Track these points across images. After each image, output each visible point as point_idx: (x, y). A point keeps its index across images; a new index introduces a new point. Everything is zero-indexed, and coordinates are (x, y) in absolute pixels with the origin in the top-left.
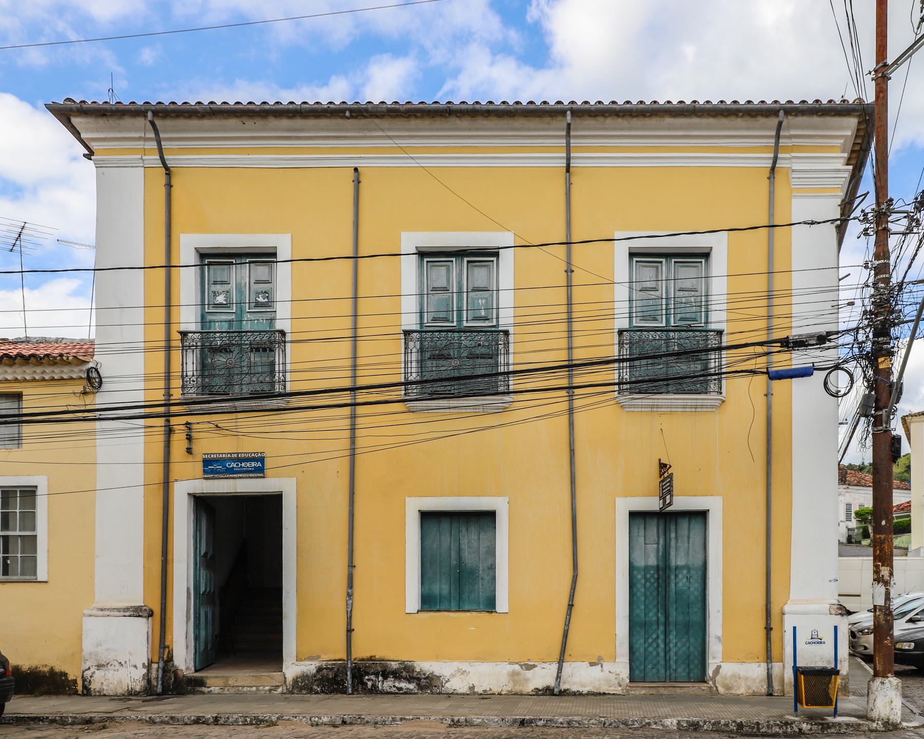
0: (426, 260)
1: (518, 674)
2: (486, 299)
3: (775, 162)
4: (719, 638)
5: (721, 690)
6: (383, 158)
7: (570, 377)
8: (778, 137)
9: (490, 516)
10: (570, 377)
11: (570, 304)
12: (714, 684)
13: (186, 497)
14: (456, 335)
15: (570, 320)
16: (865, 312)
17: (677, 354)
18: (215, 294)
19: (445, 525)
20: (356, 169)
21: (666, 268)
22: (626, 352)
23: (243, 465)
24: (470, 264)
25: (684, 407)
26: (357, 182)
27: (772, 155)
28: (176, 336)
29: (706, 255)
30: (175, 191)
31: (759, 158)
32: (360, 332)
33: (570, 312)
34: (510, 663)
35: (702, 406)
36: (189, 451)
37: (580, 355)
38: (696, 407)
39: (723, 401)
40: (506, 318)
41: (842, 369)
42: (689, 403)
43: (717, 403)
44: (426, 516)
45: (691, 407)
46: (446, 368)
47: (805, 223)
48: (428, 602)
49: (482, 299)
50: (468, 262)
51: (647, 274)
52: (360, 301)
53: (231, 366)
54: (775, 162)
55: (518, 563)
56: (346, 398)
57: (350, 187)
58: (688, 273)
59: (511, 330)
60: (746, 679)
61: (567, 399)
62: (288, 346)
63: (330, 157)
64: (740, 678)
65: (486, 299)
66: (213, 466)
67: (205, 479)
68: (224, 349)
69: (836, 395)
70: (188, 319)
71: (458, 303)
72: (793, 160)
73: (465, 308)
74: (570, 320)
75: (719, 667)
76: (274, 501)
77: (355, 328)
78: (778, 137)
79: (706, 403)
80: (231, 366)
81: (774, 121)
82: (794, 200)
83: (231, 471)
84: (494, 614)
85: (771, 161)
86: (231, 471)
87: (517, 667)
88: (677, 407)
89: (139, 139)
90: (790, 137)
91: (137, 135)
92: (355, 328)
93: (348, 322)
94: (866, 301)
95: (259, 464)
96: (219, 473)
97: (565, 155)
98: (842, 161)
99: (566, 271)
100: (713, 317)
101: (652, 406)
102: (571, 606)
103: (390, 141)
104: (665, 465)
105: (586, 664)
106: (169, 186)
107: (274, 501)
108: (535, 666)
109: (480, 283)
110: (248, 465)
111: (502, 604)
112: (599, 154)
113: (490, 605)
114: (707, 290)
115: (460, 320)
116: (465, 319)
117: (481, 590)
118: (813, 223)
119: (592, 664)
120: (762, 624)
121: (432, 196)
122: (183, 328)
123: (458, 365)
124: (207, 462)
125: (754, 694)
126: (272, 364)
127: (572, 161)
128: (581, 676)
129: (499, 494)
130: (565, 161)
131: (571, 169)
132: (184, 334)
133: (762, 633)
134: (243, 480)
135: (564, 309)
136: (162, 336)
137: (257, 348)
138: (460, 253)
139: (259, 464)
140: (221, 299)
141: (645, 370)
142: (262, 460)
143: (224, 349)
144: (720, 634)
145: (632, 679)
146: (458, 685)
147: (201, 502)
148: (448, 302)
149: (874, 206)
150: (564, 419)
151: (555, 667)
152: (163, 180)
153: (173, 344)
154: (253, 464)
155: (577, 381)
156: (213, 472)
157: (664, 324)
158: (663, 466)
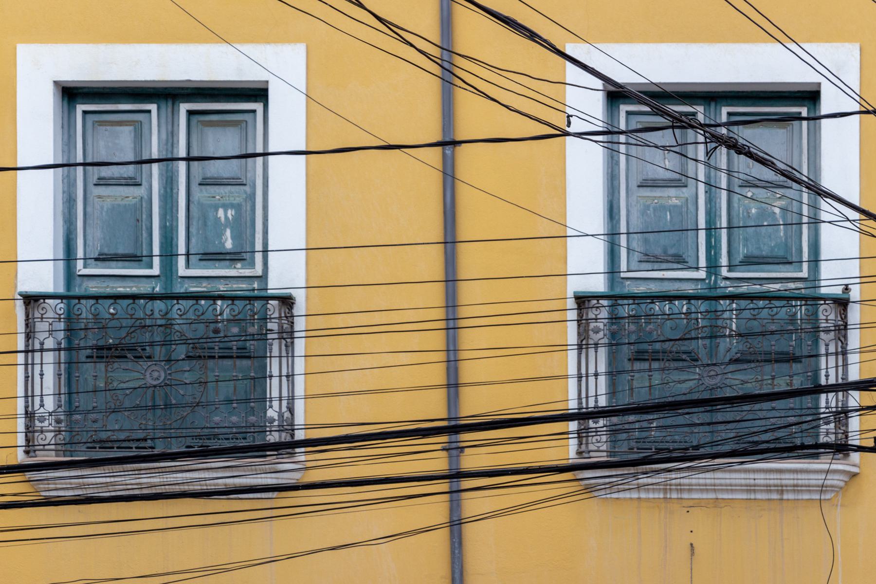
0: (80, 108)
2: (238, 207)
7: (455, 450)
10: (455, 450)
11: (451, 280)
14: (159, 305)
22: (599, 394)
24: (195, 119)
33: (451, 304)
35: (796, 488)
37: (476, 404)
38: (781, 489)
39: (854, 475)
40: (286, 272)
45: (768, 488)
49: (226, 207)
50: (190, 113)
59: (300, 297)
61: (442, 325)
65: (238, 207)
73: (182, 249)
79: (803, 479)
100: (826, 271)
115: (169, 255)
138: (167, 94)
148: (139, 214)
150: (440, 539)
155: (472, 460)
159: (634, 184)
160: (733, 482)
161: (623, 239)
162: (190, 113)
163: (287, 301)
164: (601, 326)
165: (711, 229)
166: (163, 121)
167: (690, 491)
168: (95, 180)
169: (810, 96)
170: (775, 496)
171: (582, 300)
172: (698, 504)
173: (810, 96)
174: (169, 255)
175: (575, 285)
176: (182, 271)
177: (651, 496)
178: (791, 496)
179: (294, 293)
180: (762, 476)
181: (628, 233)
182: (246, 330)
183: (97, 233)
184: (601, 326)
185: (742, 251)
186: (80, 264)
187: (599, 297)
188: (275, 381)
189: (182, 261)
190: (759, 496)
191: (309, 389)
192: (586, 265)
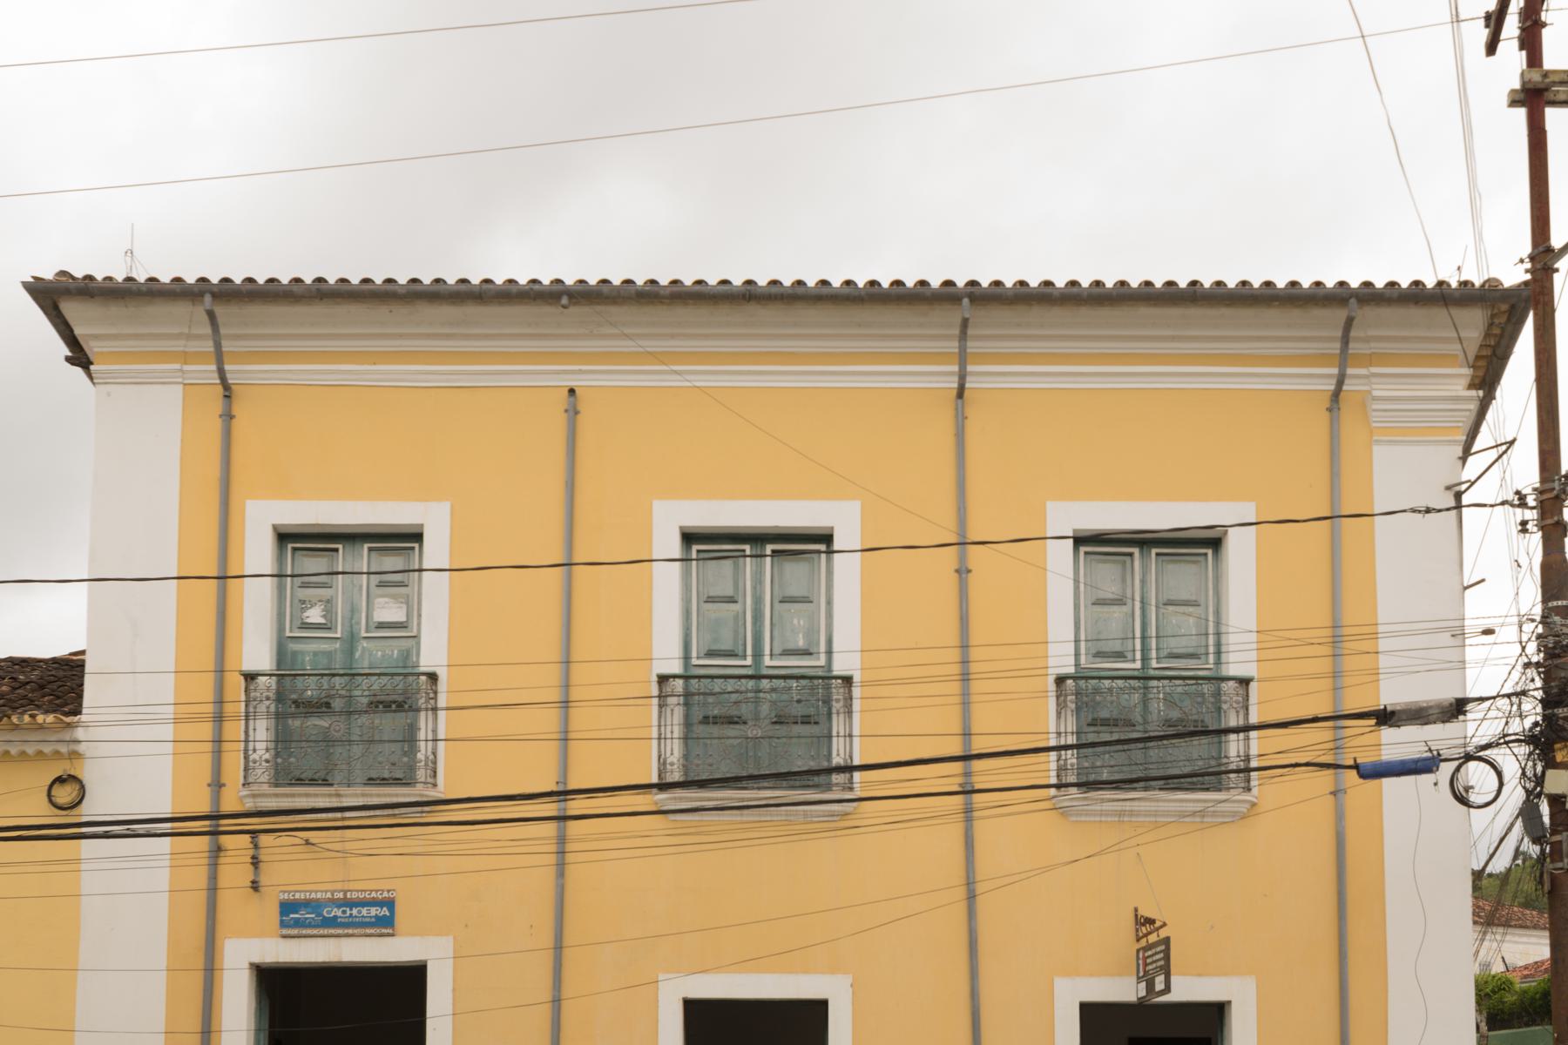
3: (1340, 382)
6: (622, 379)
7: (967, 774)
8: (1345, 340)
15: (965, 677)
16: (1527, 665)
18: (304, 604)
20: (572, 391)
23: (355, 912)
25: (1183, 815)
26: (573, 412)
27: (1335, 371)
28: (236, 685)
30: (240, 426)
32: (575, 694)
36: (255, 886)
39: (1254, 805)
40: (432, 655)
41: (1480, 759)
43: (1243, 808)
45: (1194, 814)
47: (1414, 511)
51: (1107, 577)
52: (574, 667)
53: (335, 728)
54: (1340, 382)
56: (549, 808)
57: (559, 421)
58: (1182, 577)
59: (857, 679)
62: (441, 714)
63: (520, 381)
66: (296, 915)
67: (284, 937)
68: (321, 706)
69: (1463, 800)
70: (256, 653)
71: (754, 588)
72: (1374, 380)
74: (965, 677)
76: (412, 978)
77: (567, 686)
78: (1345, 340)
80: (335, 728)
81: (1340, 314)
82: (1376, 449)
83: (332, 922)
85: (1334, 381)
86: (332, 922)
88: (1167, 814)
89: (178, 336)
90: (1367, 340)
91: (176, 331)
92: (567, 686)
93: (553, 674)
94: (1532, 647)
95: (385, 911)
96: (310, 926)
97: (956, 368)
98: (1465, 382)
99: (957, 571)
101: (1121, 813)
103: (631, 343)
104: (1151, 921)
106: (228, 416)
107: (412, 978)
109: (793, 591)
110: (364, 911)
112: (1013, 377)
115: (758, 655)
116: (767, 651)
118: (1428, 511)
121: (703, 451)
122: (249, 666)
123: (758, 738)
124: (287, 907)
126: (413, 729)
127: (968, 379)
129: (833, 970)
130: (956, 379)
131: (966, 393)
132: (250, 677)
134: (350, 940)
135: (955, 655)
136: (209, 695)
137: (382, 704)
139: (385, 911)
140: (315, 615)
141: (1107, 765)
142: (390, 904)
143: (321, 706)
147: (275, 984)
152: (218, 406)
153: (229, 708)
154: (374, 911)
156: (298, 924)
157: (1138, 665)
158: (1144, 923)
161: (1211, 650)
163: (433, 677)
165: (1144, 638)
169: (826, 538)
171: (663, 679)
173: (826, 538)
175: (1054, 671)
182: (819, 696)
185: (1165, 652)
187: (675, 677)
188: (676, 735)
191: (858, 736)
192: (1062, 659)
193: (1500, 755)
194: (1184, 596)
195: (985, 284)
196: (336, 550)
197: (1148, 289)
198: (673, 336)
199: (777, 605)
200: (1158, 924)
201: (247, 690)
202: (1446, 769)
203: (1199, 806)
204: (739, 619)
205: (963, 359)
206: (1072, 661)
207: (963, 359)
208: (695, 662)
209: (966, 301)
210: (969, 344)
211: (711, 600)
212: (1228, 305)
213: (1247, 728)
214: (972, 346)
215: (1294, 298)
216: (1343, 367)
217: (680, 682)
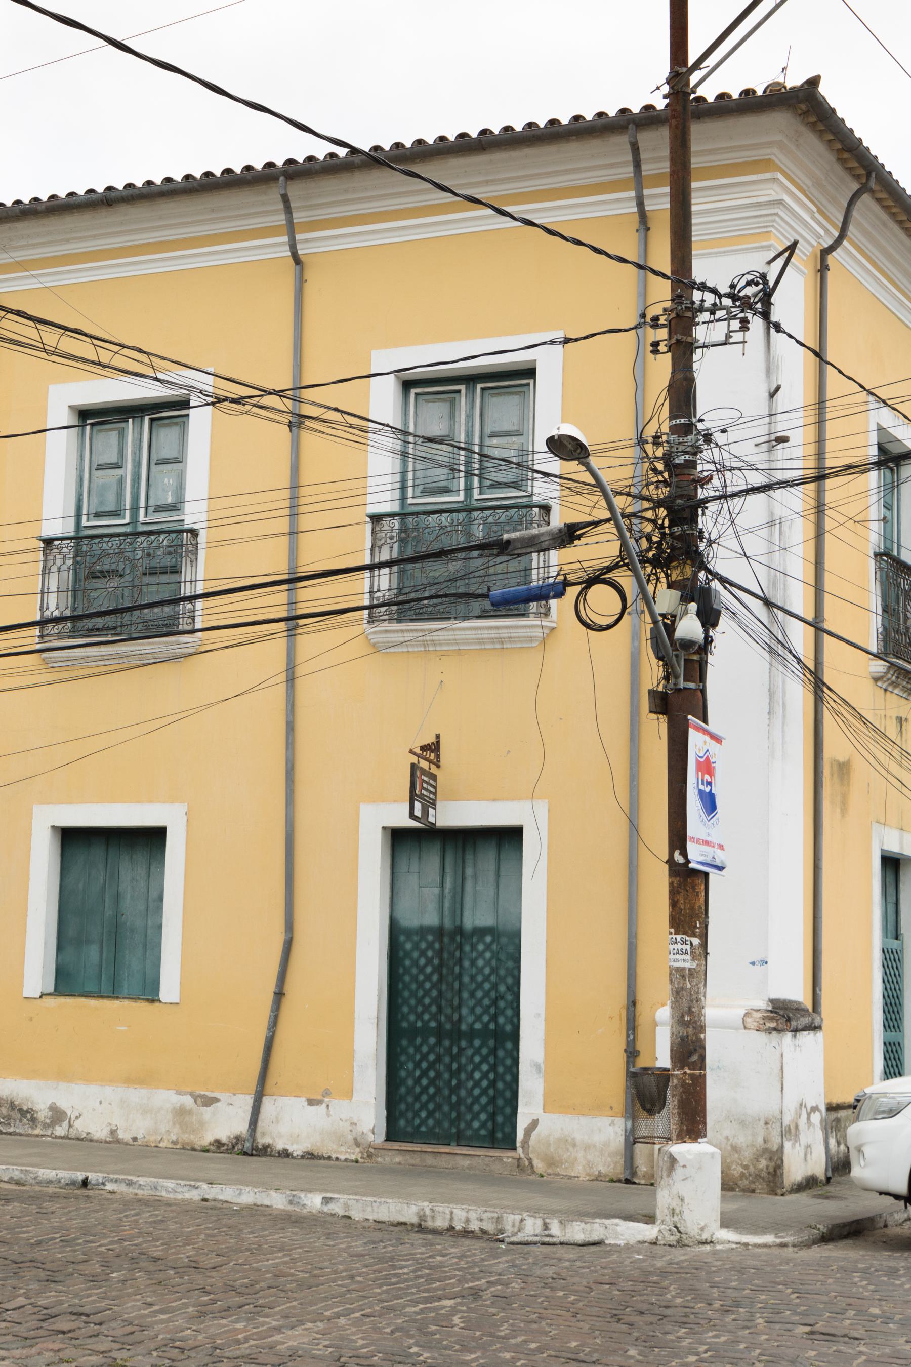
1: (190, 1112)
3: (640, 204)
4: (538, 1067)
5: (539, 1165)
8: (637, 165)
9: (153, 838)
12: (527, 1154)
13: (380, 830)
17: (481, 547)
19: (97, 852)
21: (465, 401)
25: (480, 641)
29: (530, 372)
31: (618, 200)
34: (179, 1093)
38: (501, 641)
39: (553, 629)
40: (194, 514)
41: (605, 582)
42: (485, 634)
43: (538, 633)
44: (71, 838)
45: (492, 641)
46: (103, 595)
48: (66, 982)
54: (640, 204)
55: (194, 916)
56: (274, 602)
60: (587, 1148)
64: (574, 1145)
75: (535, 1124)
78: (637, 165)
79: (515, 633)
84: (157, 1004)
87: (188, 1101)
88: (467, 642)
97: (285, 239)
102: (279, 995)
105: (303, 1101)
108: (216, 1100)
109: (166, 453)
111: (169, 989)
113: (149, 991)
114: (404, 463)
115: (135, 509)
117: (132, 961)
119: (311, 1102)
120: (271, 987)
125: (598, 1178)
127: (646, 202)
128: (293, 1123)
129: (172, 800)
133: (269, 997)
144: (539, 1057)
145: (389, 1137)
146: (94, 1125)
149: (668, 305)
151: (249, 1100)
157: (461, 497)
159: (95, 466)
160: (467, 637)
161: (410, 475)
162: (417, 394)
163: (194, 533)
164: (395, 534)
166: (136, 431)
167: (440, 645)
168: (155, 461)
170: (498, 646)
171: (376, 519)
172: (447, 653)
174: (135, 509)
176: (141, 517)
177: (416, 649)
178: (509, 646)
179: (551, 503)
180: (486, 632)
181: (414, 471)
183: (95, 500)
184: (395, 534)
186: (84, 518)
189: (142, 512)
190: (488, 646)
193: (615, 575)
194: (506, 427)
195: (218, 173)
196: (459, 391)
197: (444, 143)
198: (68, 241)
199: (153, 466)
200: (414, 759)
201: (374, 532)
202: (572, 592)
203: (493, 634)
204: (121, 482)
205: (291, 229)
206: (72, 522)
207: (291, 229)
208: (410, 501)
209: (282, 178)
210: (295, 215)
211: (101, 467)
212: (529, 146)
213: (371, 567)
214: (298, 217)
215: (580, 131)
216: (639, 188)
217: (396, 523)
